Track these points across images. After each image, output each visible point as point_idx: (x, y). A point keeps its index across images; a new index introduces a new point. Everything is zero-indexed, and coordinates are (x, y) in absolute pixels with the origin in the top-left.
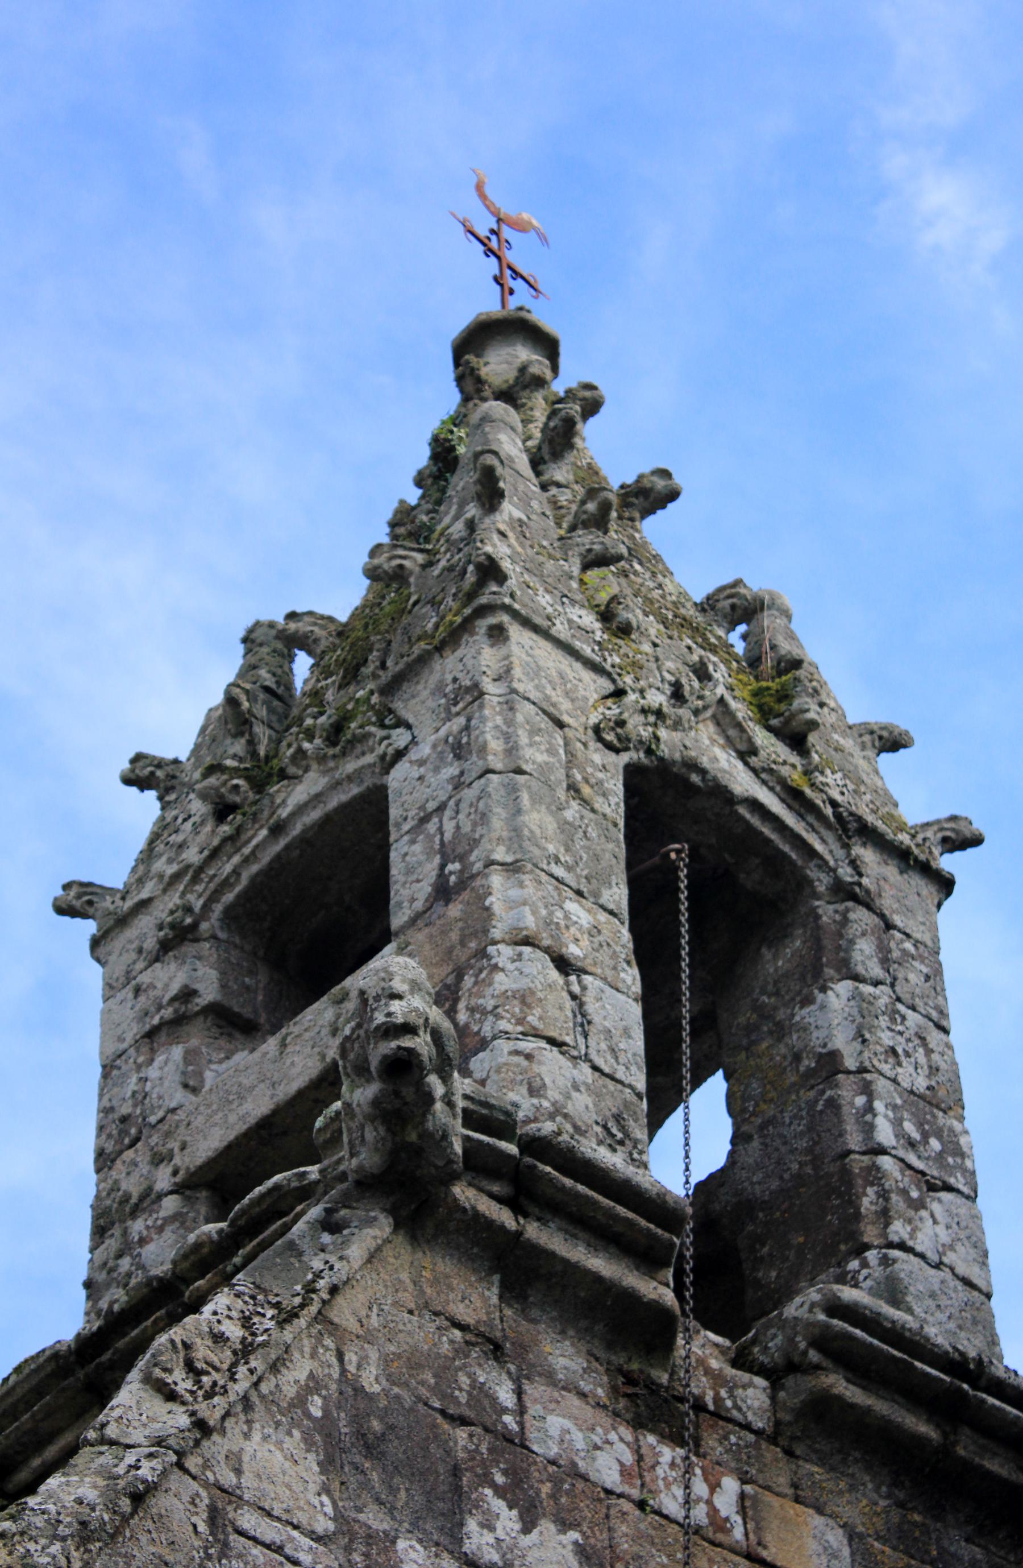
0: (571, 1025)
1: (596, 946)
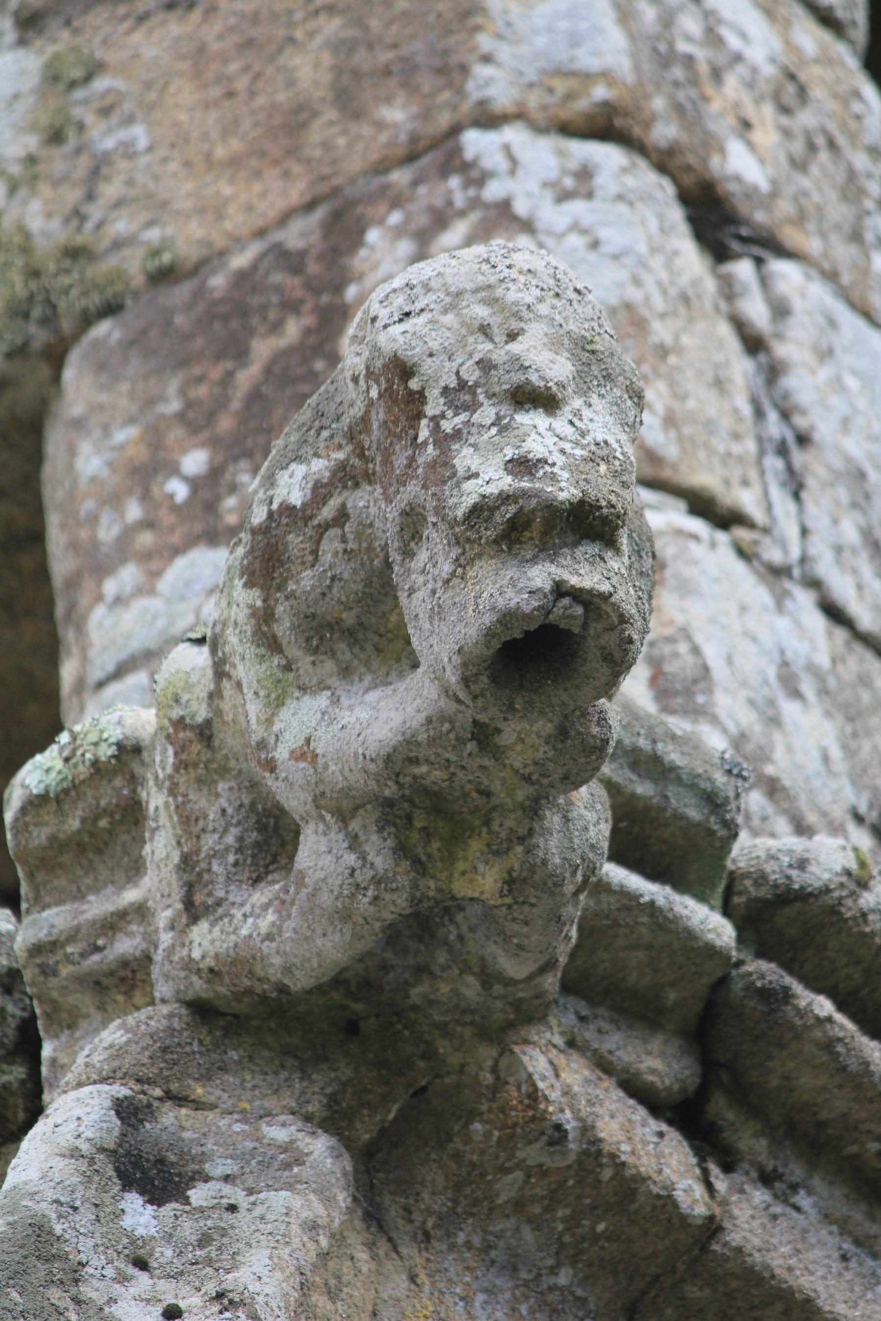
0: (750, 446)
1: (798, 147)
